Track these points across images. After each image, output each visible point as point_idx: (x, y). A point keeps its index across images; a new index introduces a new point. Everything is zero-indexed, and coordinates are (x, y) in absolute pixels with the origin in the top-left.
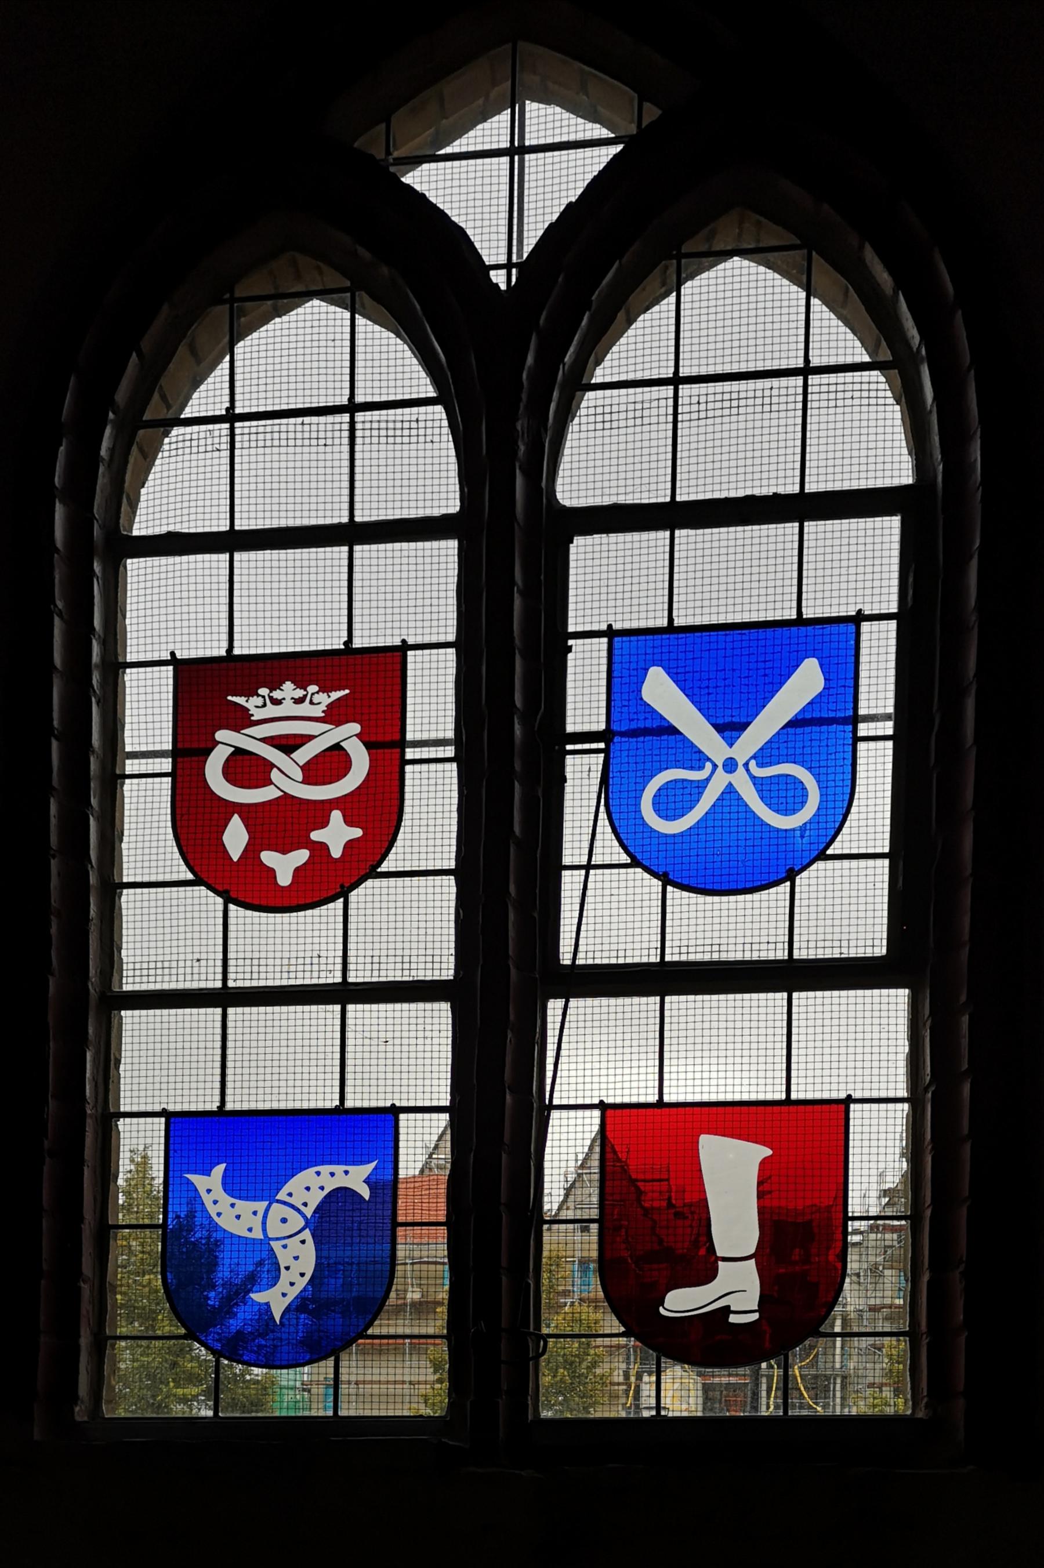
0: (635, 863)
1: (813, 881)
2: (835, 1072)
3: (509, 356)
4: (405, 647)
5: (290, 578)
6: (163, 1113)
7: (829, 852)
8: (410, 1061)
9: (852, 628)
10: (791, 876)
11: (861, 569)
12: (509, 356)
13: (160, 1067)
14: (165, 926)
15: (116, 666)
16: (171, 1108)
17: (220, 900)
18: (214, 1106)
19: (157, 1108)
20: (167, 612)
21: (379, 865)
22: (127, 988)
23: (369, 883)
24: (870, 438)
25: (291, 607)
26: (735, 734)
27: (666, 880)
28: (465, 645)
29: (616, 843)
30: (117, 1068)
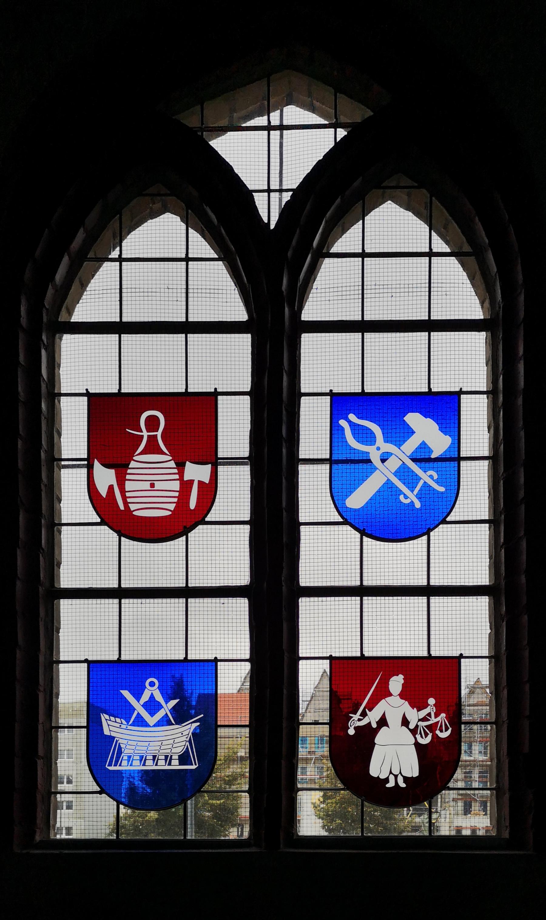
0: (346, 522)
1: (441, 534)
2: (446, 625)
3: (273, 261)
4: (216, 394)
5: (477, 445)
6: (86, 661)
7: (448, 519)
8: (224, 637)
9: (213, 398)
10: (427, 533)
11: (464, 363)
12: (273, 261)
13: (83, 634)
14: (85, 552)
15: (54, 396)
16: (90, 658)
17: (115, 535)
18: (115, 658)
19: (83, 659)
20: (84, 367)
21: (206, 516)
22: (62, 587)
23: (200, 527)
24: (458, 293)
25: (154, 368)
26: (97, 264)
27: (363, 533)
28: (255, 394)
29: (333, 506)
30: (58, 632)
